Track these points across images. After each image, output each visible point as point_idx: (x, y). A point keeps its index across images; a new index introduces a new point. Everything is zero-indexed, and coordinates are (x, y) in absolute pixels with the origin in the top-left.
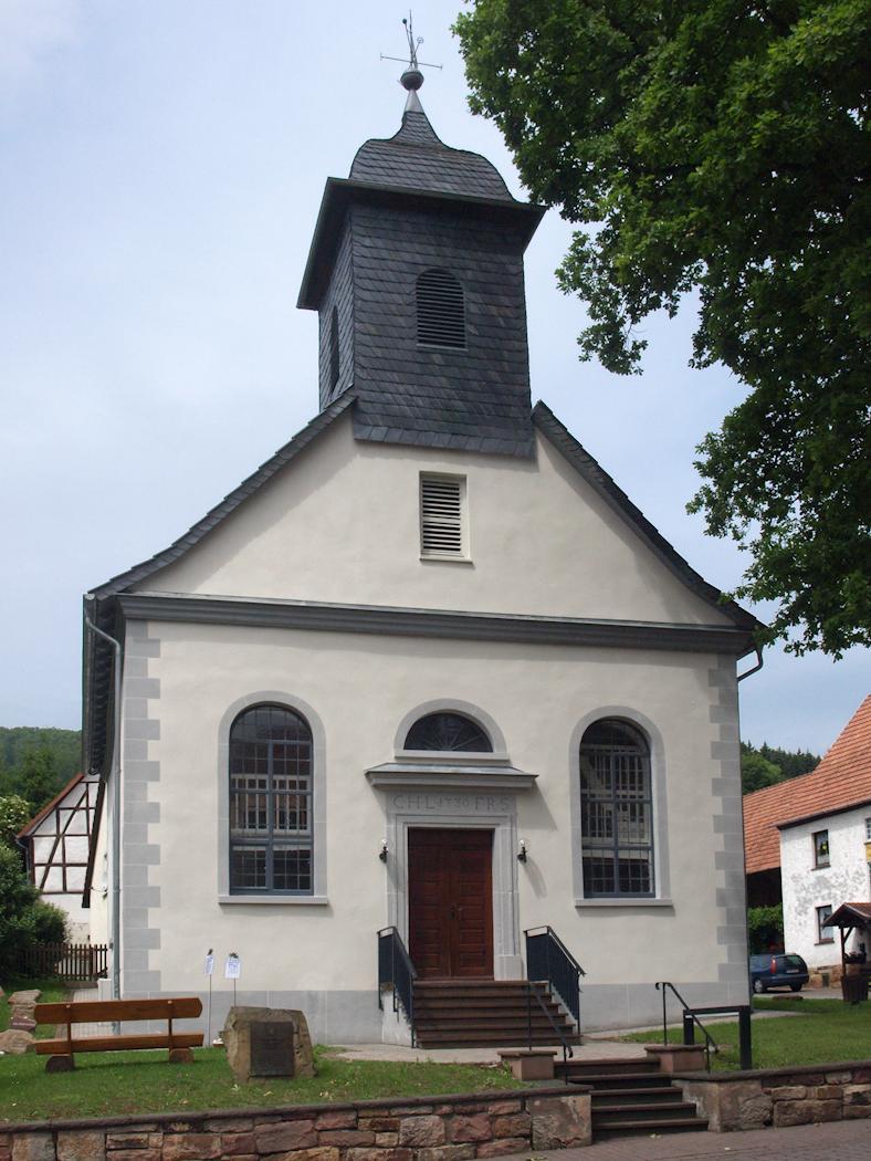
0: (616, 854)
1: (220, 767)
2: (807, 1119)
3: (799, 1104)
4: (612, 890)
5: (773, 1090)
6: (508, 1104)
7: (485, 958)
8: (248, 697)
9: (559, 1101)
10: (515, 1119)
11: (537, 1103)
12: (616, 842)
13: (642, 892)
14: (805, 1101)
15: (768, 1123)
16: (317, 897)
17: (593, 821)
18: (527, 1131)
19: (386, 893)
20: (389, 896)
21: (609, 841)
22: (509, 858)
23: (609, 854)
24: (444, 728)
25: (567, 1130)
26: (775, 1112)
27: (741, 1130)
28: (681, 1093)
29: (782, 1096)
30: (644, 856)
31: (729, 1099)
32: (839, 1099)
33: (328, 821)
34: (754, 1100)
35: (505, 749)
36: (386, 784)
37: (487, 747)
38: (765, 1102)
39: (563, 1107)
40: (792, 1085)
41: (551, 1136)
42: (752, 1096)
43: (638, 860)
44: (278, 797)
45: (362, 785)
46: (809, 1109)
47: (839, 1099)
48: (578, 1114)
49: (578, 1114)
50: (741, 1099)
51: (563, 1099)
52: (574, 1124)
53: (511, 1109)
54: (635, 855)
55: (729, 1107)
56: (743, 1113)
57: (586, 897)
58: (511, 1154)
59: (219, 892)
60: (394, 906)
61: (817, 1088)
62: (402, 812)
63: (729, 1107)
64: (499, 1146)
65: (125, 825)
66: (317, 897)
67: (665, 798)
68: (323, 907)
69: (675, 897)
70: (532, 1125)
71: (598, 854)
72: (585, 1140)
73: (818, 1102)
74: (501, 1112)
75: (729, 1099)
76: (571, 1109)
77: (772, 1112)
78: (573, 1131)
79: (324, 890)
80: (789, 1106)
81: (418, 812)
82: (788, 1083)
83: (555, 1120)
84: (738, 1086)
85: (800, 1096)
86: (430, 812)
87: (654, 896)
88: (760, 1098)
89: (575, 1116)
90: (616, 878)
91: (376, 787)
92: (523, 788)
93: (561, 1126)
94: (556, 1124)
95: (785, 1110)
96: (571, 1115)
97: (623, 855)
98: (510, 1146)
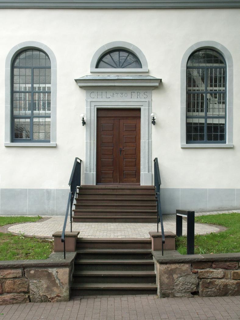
0: (206, 121)
1: (6, 80)
2: (224, 292)
3: (218, 282)
4: (203, 140)
5: (199, 271)
6: (13, 271)
7: (137, 175)
8: (19, 45)
9: (46, 271)
10: (18, 281)
11: (32, 272)
12: (206, 114)
13: (219, 141)
14: (223, 280)
15: (195, 293)
16: (52, 143)
17: (194, 102)
18: (26, 290)
19: (85, 141)
20: (87, 142)
21: (203, 114)
22: (147, 123)
23: (202, 121)
24: (118, 55)
25: (52, 291)
26: (200, 286)
27: (174, 296)
28: (154, 265)
29: (206, 275)
30: (222, 121)
31: (167, 276)
32: (25, 293)
33: (58, 106)
34: (185, 278)
35: (148, 66)
36: (87, 86)
37: (141, 67)
38: (193, 279)
39: (50, 275)
40: (214, 268)
41: (41, 294)
42: (184, 274)
43: (217, 124)
44: (222, 94)
45: (75, 87)
46: (226, 286)
47: (25, 293)
48: (59, 280)
49: (59, 280)
50: (175, 276)
51: (50, 270)
52: (57, 287)
53: (15, 275)
54: (216, 121)
55: (166, 281)
56: (177, 285)
57: (187, 143)
58: (13, 304)
59: (5, 141)
60: (89, 147)
61: (233, 272)
62: (94, 100)
63: (166, 281)
64: (6, 298)
65: (228, 107)
66: (52, 143)
67: (232, 89)
68: (55, 147)
69: (235, 143)
70: (29, 286)
71: (196, 121)
72: (64, 297)
73: (233, 281)
74: (8, 277)
75: (167, 276)
76: (55, 276)
77: (198, 286)
78: (56, 291)
79: (55, 140)
80: (210, 282)
81: (101, 100)
82: (211, 267)
83: (44, 283)
84: (173, 266)
85: (219, 276)
86: (108, 100)
87: (225, 143)
88: (189, 276)
89: (57, 282)
90: (205, 133)
91: (81, 87)
92: (157, 85)
93: (48, 288)
94: (45, 286)
95: (208, 285)
96: (55, 281)
97: (210, 121)
98: (14, 299)
